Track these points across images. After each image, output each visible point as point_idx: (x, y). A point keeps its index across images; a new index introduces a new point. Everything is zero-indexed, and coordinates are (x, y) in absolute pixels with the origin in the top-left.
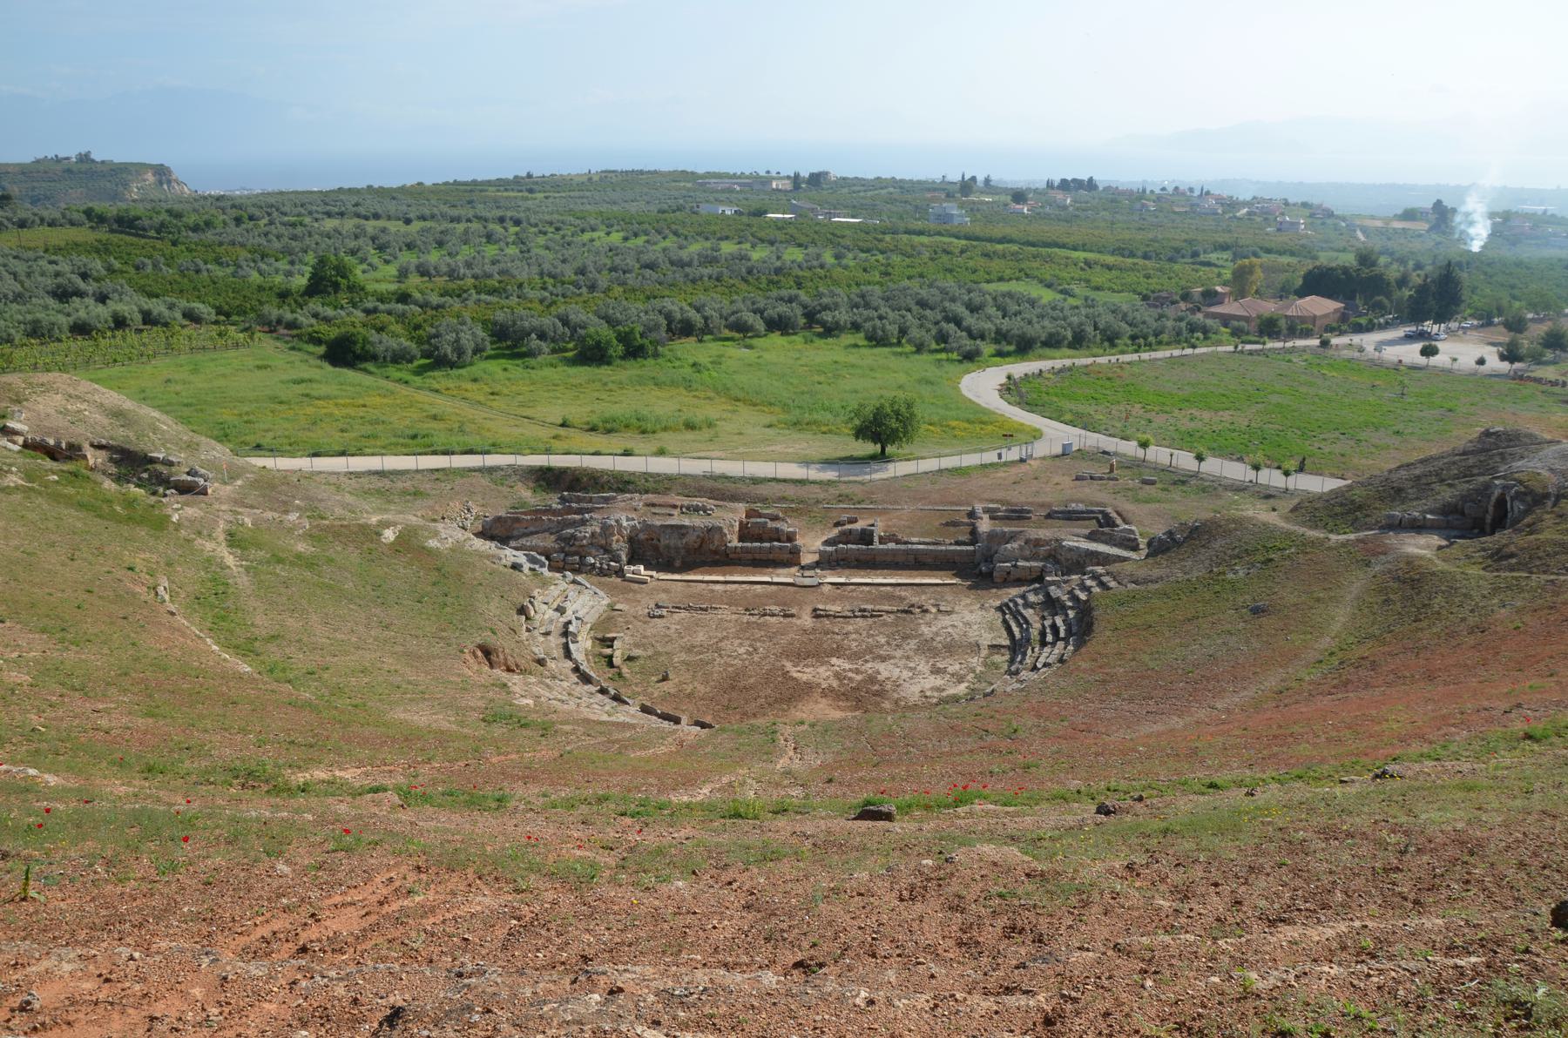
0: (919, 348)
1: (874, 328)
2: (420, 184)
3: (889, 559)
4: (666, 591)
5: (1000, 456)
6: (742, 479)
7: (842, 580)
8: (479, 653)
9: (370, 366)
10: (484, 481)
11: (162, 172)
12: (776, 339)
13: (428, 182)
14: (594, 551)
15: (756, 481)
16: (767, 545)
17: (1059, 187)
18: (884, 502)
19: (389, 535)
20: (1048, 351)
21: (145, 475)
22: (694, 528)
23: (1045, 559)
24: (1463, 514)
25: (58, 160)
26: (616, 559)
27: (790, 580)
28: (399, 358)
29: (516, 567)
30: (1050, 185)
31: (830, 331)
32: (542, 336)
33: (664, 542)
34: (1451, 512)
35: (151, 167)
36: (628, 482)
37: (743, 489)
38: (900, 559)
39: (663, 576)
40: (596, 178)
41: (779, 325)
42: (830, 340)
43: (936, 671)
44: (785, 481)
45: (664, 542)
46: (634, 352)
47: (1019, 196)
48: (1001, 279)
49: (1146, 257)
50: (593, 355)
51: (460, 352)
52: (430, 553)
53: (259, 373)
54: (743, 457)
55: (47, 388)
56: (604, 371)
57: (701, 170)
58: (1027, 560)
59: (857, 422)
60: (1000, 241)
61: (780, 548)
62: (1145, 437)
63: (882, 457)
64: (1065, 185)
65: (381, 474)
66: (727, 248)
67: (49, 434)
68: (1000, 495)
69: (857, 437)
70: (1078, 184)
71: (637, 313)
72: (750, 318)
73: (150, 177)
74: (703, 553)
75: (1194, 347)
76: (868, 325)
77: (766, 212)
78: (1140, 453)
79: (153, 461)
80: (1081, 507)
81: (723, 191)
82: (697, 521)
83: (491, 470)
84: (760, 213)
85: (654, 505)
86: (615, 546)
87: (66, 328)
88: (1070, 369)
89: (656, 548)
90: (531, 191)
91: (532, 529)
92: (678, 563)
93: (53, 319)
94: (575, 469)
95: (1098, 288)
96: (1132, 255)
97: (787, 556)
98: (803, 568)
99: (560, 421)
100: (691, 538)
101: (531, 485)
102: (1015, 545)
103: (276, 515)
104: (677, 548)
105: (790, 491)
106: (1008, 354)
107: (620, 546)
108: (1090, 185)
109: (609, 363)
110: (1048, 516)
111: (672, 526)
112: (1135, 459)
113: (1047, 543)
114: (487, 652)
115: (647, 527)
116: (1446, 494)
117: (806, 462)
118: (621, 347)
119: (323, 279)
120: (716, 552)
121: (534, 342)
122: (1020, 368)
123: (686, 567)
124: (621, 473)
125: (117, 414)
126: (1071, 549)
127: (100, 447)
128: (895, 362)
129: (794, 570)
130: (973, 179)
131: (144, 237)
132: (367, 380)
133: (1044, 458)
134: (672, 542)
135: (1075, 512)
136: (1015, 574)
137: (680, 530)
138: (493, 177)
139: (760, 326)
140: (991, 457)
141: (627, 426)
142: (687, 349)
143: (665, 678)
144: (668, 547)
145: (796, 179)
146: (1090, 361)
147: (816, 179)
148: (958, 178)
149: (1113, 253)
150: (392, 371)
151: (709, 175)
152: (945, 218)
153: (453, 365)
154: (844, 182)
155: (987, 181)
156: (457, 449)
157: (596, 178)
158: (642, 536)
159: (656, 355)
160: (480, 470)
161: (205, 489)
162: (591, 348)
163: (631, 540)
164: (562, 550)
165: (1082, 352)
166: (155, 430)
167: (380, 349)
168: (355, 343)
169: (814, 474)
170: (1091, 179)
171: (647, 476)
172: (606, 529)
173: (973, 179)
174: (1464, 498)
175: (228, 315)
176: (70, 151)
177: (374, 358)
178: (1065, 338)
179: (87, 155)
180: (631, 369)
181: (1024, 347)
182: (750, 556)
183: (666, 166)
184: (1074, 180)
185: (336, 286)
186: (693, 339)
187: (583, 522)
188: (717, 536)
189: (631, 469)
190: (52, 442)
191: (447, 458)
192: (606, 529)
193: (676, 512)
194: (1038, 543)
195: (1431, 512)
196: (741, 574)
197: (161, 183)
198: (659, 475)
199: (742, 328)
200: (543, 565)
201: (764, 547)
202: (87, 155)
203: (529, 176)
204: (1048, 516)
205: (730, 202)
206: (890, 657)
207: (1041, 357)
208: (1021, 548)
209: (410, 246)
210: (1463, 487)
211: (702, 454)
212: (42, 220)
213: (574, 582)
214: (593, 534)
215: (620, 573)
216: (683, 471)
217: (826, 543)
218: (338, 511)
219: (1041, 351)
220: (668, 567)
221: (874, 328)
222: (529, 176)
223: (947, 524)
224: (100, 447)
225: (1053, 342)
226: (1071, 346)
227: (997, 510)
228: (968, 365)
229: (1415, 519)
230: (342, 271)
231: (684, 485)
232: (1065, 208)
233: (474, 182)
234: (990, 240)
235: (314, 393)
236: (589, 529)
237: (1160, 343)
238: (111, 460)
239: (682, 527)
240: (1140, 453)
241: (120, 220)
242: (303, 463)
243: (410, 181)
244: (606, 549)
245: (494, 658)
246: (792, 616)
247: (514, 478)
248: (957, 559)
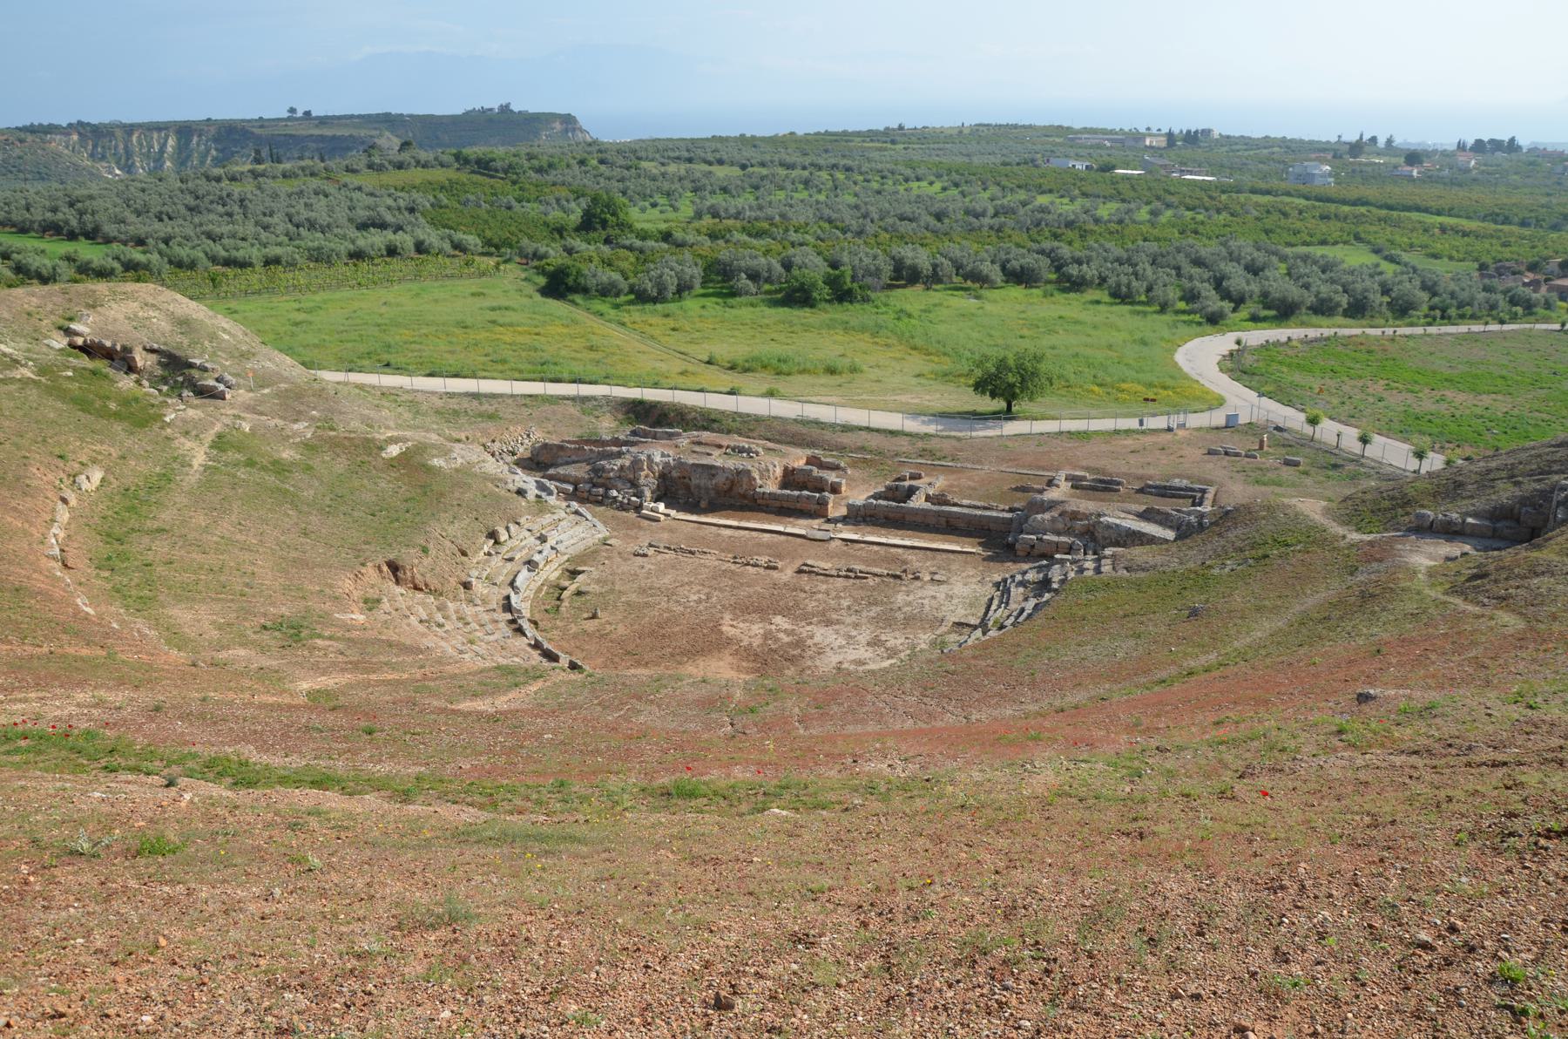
0: (1163, 308)
1: (1118, 285)
2: (792, 133)
3: (919, 519)
4: (671, 531)
5: (1141, 423)
6: (833, 426)
7: (855, 537)
8: (385, 568)
9: (578, 298)
10: (573, 410)
11: (568, 121)
12: (1017, 292)
13: (800, 132)
14: (619, 485)
15: (847, 428)
16: (796, 493)
17: (1472, 149)
18: (967, 460)
19: (394, 450)
20: (1315, 319)
21: (180, 379)
22: (723, 469)
23: (1080, 536)
24: (1518, 521)
25: (483, 111)
26: (639, 495)
27: (803, 532)
28: (606, 291)
29: (521, 492)
30: (1461, 146)
31: (1075, 285)
32: (754, 276)
33: (695, 481)
34: (1506, 518)
35: (560, 116)
36: (714, 421)
37: (828, 435)
38: (932, 521)
39: (682, 516)
40: (966, 132)
41: (1021, 277)
42: (1072, 295)
43: (875, 643)
44: (878, 430)
45: (695, 481)
46: (842, 296)
47: (1413, 157)
48: (1323, 243)
49: (1524, 224)
50: (797, 296)
51: (662, 289)
52: (430, 470)
53: (476, 299)
54: (863, 405)
55: (128, 296)
56: (805, 313)
57: (1077, 126)
58: (1059, 534)
59: (978, 373)
60: (1354, 203)
61: (808, 497)
62: (1315, 412)
63: (1008, 415)
64: (1479, 146)
65: (476, 396)
66: (1043, 200)
67: (107, 337)
68: (1092, 463)
69: (976, 389)
70: (1496, 145)
71: (858, 255)
72: (987, 268)
73: (558, 126)
74: (733, 496)
75: (1502, 322)
76: (1112, 281)
77: (1114, 167)
78: (1308, 430)
79: (191, 366)
80: (1185, 483)
81: (1091, 147)
82: (732, 463)
83: (584, 399)
84: (1107, 168)
85: (699, 443)
86: (642, 481)
87: (344, 253)
88: (1328, 339)
89: (688, 487)
90: (893, 142)
91: (574, 458)
92: (703, 504)
93: (332, 245)
94: (666, 404)
95: (1435, 256)
96: (1507, 221)
97: (814, 507)
98: (829, 521)
99: (706, 359)
100: (720, 479)
101: (620, 416)
102: (1047, 516)
103: (281, 423)
104: (707, 489)
105: (874, 441)
106: (1265, 319)
107: (648, 481)
108: (1512, 146)
109: (812, 306)
110: (1141, 491)
111: (703, 466)
112: (1303, 437)
113: (1086, 517)
114: (394, 568)
115: (680, 465)
116: (1505, 493)
117: (916, 414)
118: (827, 289)
119: (594, 216)
120: (744, 496)
121: (743, 281)
122: (1256, 336)
123: (712, 509)
124: (710, 411)
125: (184, 323)
126: (1109, 526)
127: (152, 351)
128: (1137, 322)
129: (816, 523)
130: (1374, 140)
131: (492, 177)
132: (579, 314)
133: (1199, 429)
134: (703, 482)
135: (1171, 488)
136: (1040, 549)
137: (710, 470)
138: (864, 129)
139: (996, 274)
140: (1133, 423)
141: (765, 367)
142: (912, 298)
143: (594, 616)
144: (698, 487)
145: (1170, 135)
146: (1358, 331)
147: (1192, 138)
148: (1354, 138)
149: (1484, 219)
150: (598, 305)
151: (1085, 130)
152: (1306, 178)
153: (654, 300)
154: (1227, 140)
155: (1389, 141)
156: (566, 376)
157: (966, 132)
158: (675, 474)
159: (866, 300)
160: (573, 399)
161: (223, 393)
162: (795, 290)
163: (663, 476)
164: (590, 481)
165: (1364, 322)
166: (213, 337)
167: (591, 283)
168: (568, 275)
169: (912, 425)
170: (1513, 140)
171: (736, 415)
172: (636, 464)
173: (1374, 140)
174: (1524, 501)
175: (497, 247)
176: (493, 103)
177: (585, 291)
178: (1338, 305)
179: (508, 106)
180: (837, 313)
181: (1284, 312)
182: (778, 504)
183: (1041, 121)
184: (1492, 141)
185: (604, 224)
186: (919, 287)
187: (619, 455)
188: (745, 480)
189: (722, 407)
190: (108, 344)
191: (574, 386)
192: (636, 464)
193: (716, 452)
194: (1075, 516)
195: (1475, 515)
196: (759, 521)
197: (566, 131)
198: (748, 415)
199: (980, 279)
200: (550, 493)
201: (802, 496)
202: (508, 106)
203: (901, 128)
204: (1141, 491)
205: (1078, 157)
206: (838, 622)
207: (1303, 324)
208: (1053, 520)
209: (725, 190)
210: (1531, 486)
211: (823, 399)
212: (418, 162)
213: (577, 513)
214: (622, 467)
215: (638, 508)
216: (773, 414)
217: (876, 496)
218: (355, 424)
219: (1305, 318)
220: (693, 508)
221: (1118, 285)
222: (901, 128)
223: (1017, 489)
224: (152, 351)
225: (1323, 308)
226: (1346, 314)
227: (1083, 478)
228: (1208, 328)
229: (1450, 523)
230: (611, 207)
231: (769, 428)
232: (1468, 171)
233: (845, 133)
234: (1344, 202)
235: (501, 321)
236: (619, 462)
237: (1462, 317)
238: (160, 363)
239: (712, 467)
240: (1308, 430)
241: (479, 162)
242: (1097, 425)
243: (783, 131)
244: (634, 484)
245: (400, 574)
246: (775, 568)
247: (605, 409)
248: (992, 526)
